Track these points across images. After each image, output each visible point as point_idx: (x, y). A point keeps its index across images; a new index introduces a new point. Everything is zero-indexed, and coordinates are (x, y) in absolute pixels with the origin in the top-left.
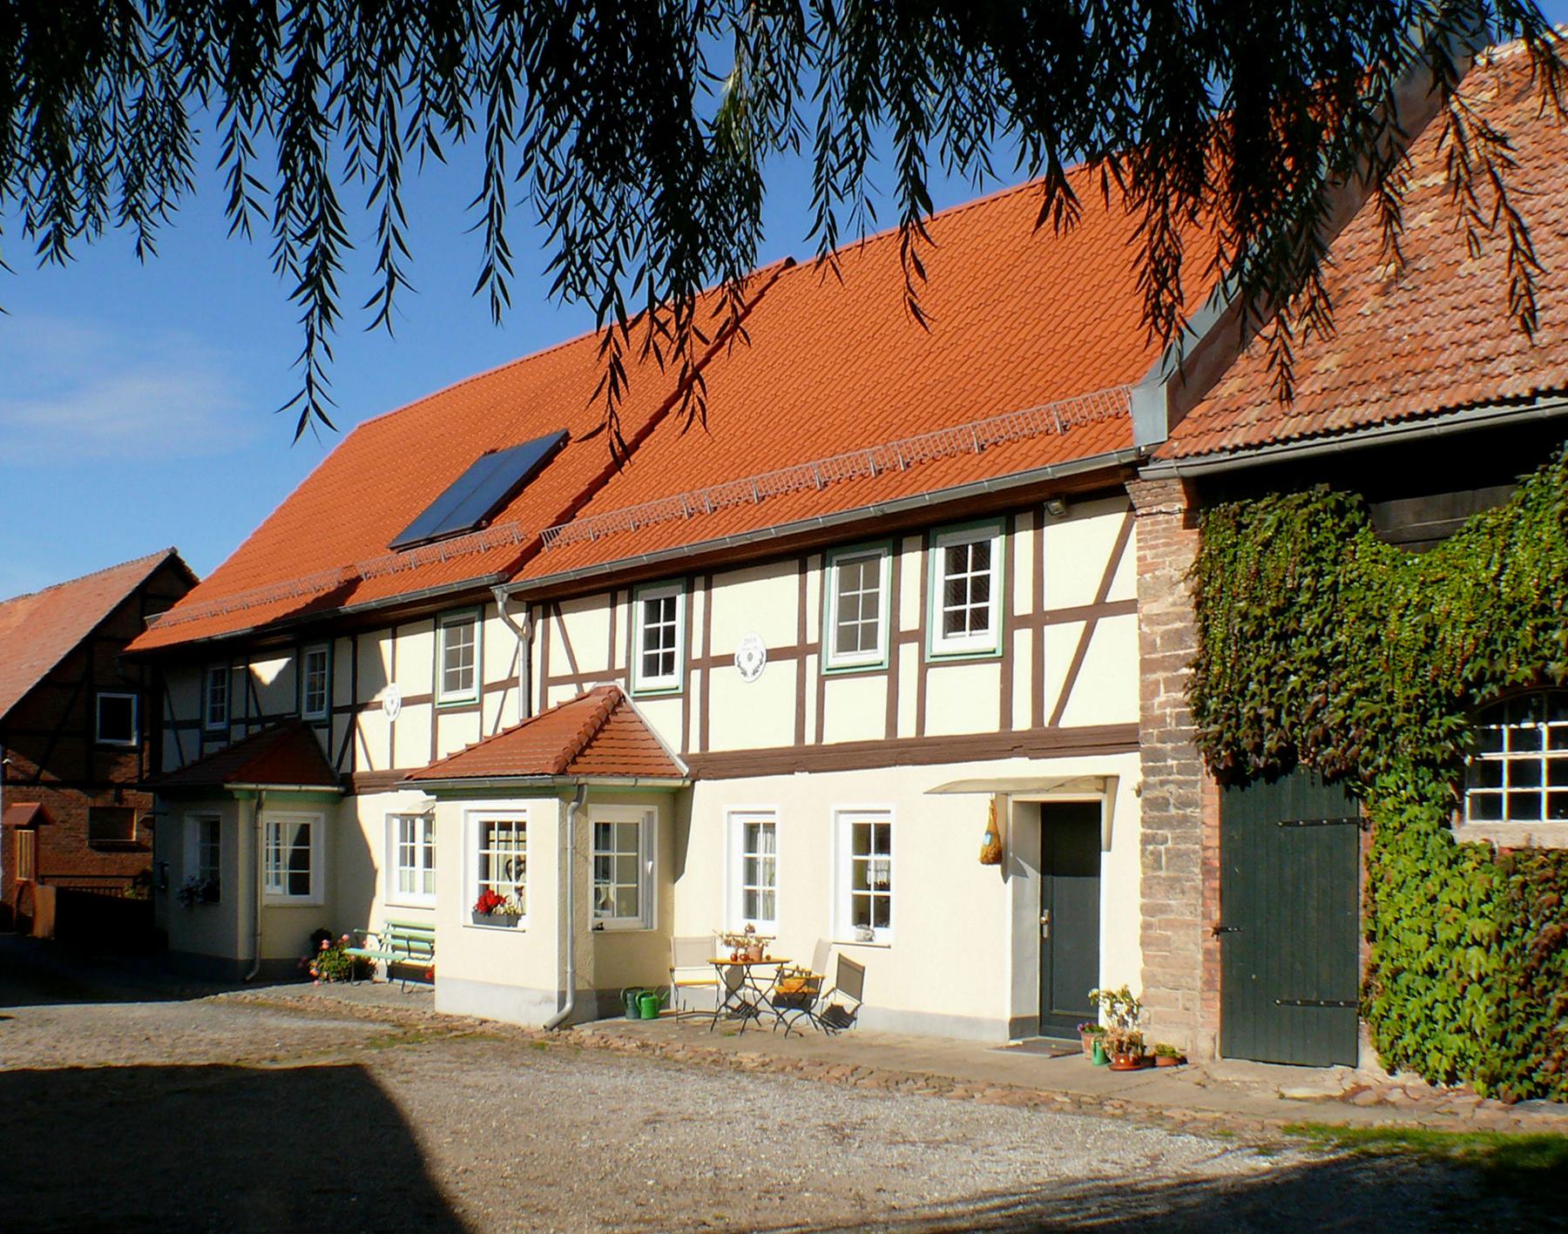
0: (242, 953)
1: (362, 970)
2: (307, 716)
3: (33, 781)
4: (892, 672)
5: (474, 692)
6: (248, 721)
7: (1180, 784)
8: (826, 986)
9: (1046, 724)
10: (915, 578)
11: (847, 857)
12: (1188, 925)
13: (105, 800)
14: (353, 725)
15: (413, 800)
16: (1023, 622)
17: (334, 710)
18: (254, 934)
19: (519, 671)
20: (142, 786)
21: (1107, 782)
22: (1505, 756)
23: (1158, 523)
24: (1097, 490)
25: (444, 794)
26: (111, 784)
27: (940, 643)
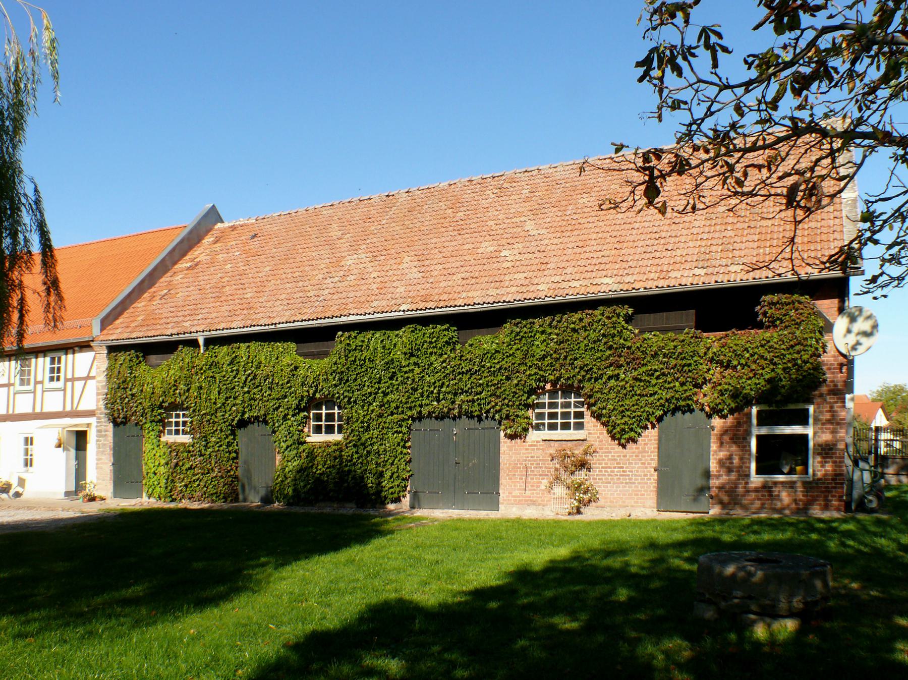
8: (13, 487)
11: (22, 447)
16: (69, 380)
21: (88, 425)
22: (559, 410)
24: (85, 346)
27: (48, 385)
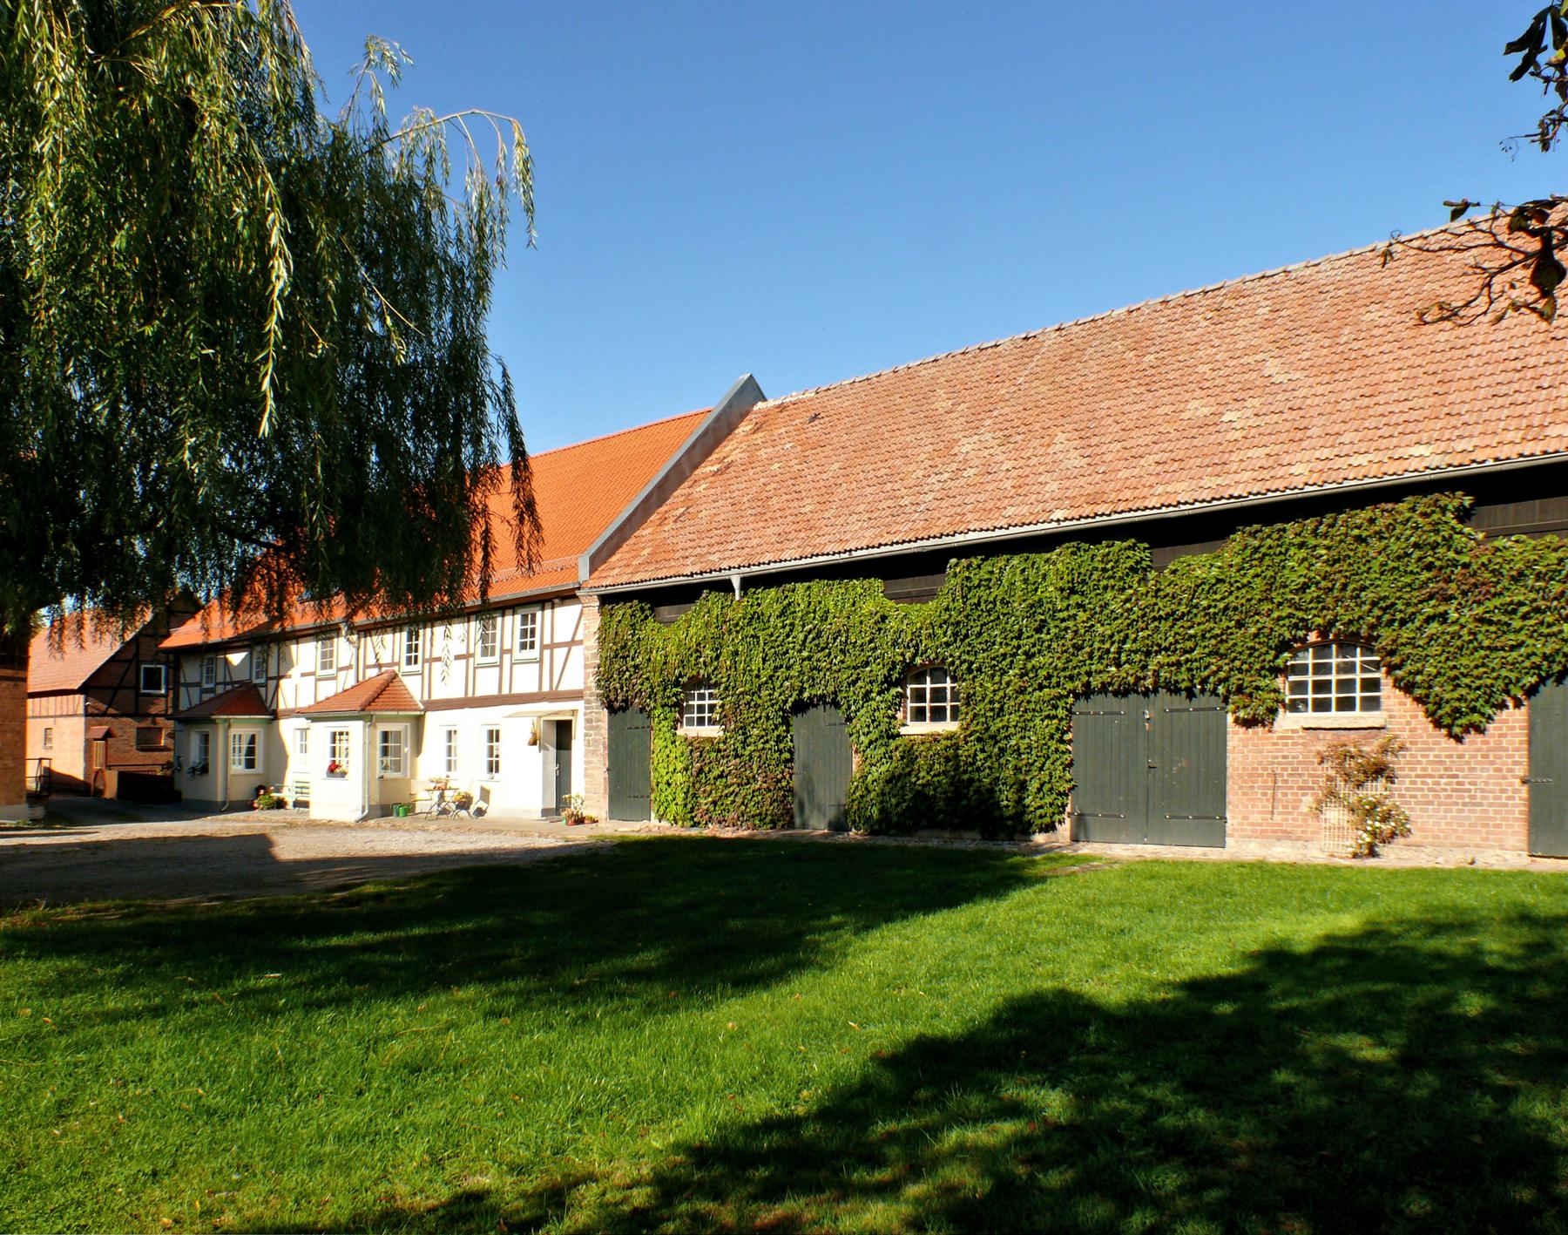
0: (220, 798)
1: (280, 804)
2: (255, 681)
3: (104, 714)
5: (333, 671)
6: (225, 684)
13: (147, 723)
14: (277, 686)
15: (302, 722)
16: (547, 647)
17: (268, 679)
18: (226, 789)
19: (354, 662)
20: (168, 717)
21: (574, 712)
24: (568, 597)
25: (314, 720)
26: (149, 715)
27: (518, 654)
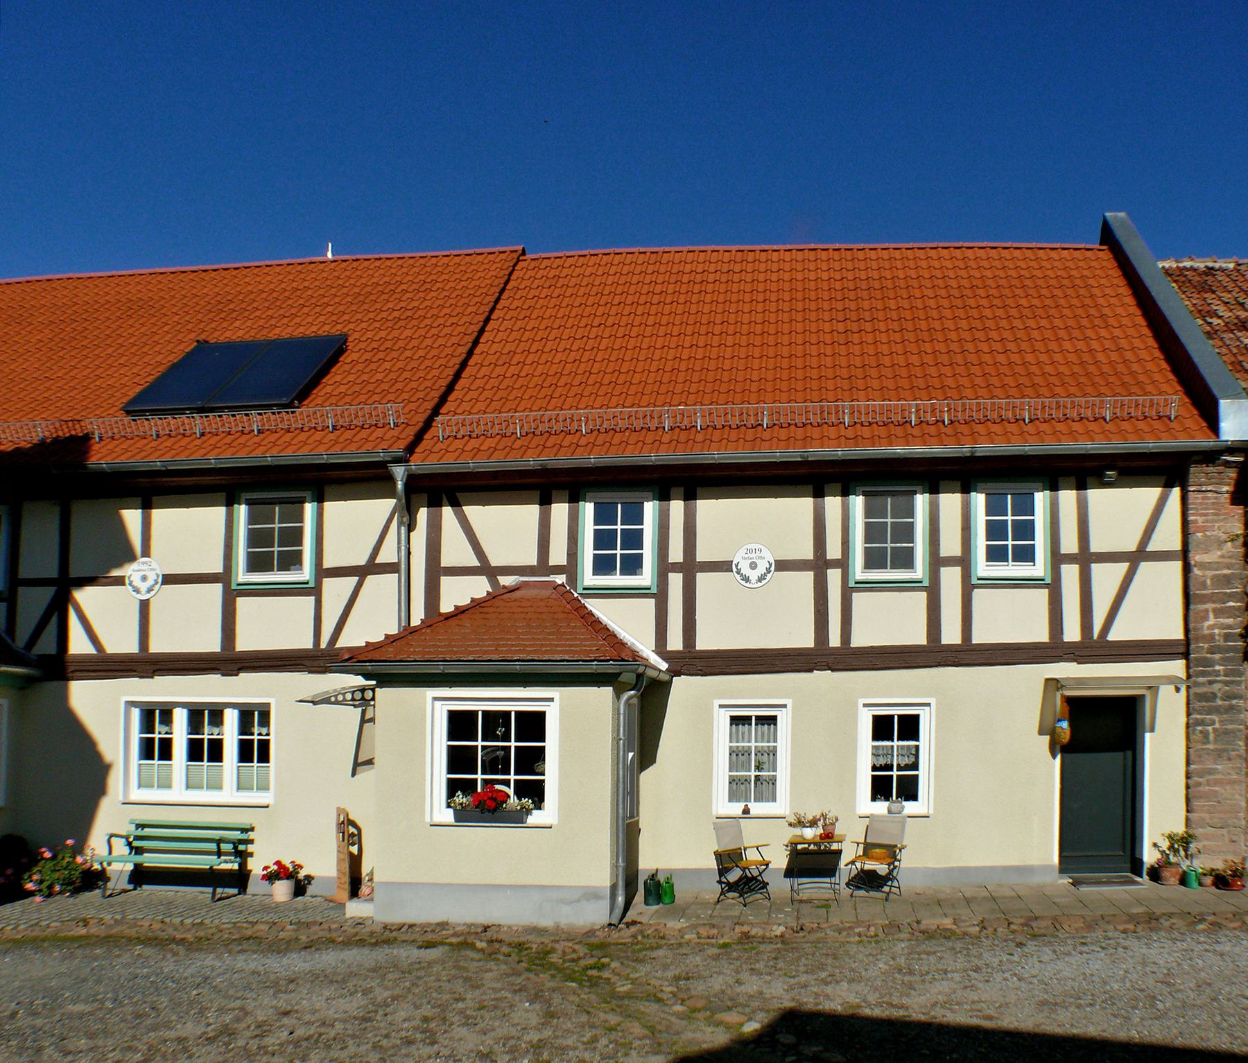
4: (661, 597)
7: (1226, 683)
9: (1095, 637)
10: (953, 515)
12: (1234, 782)
23: (1208, 498)
